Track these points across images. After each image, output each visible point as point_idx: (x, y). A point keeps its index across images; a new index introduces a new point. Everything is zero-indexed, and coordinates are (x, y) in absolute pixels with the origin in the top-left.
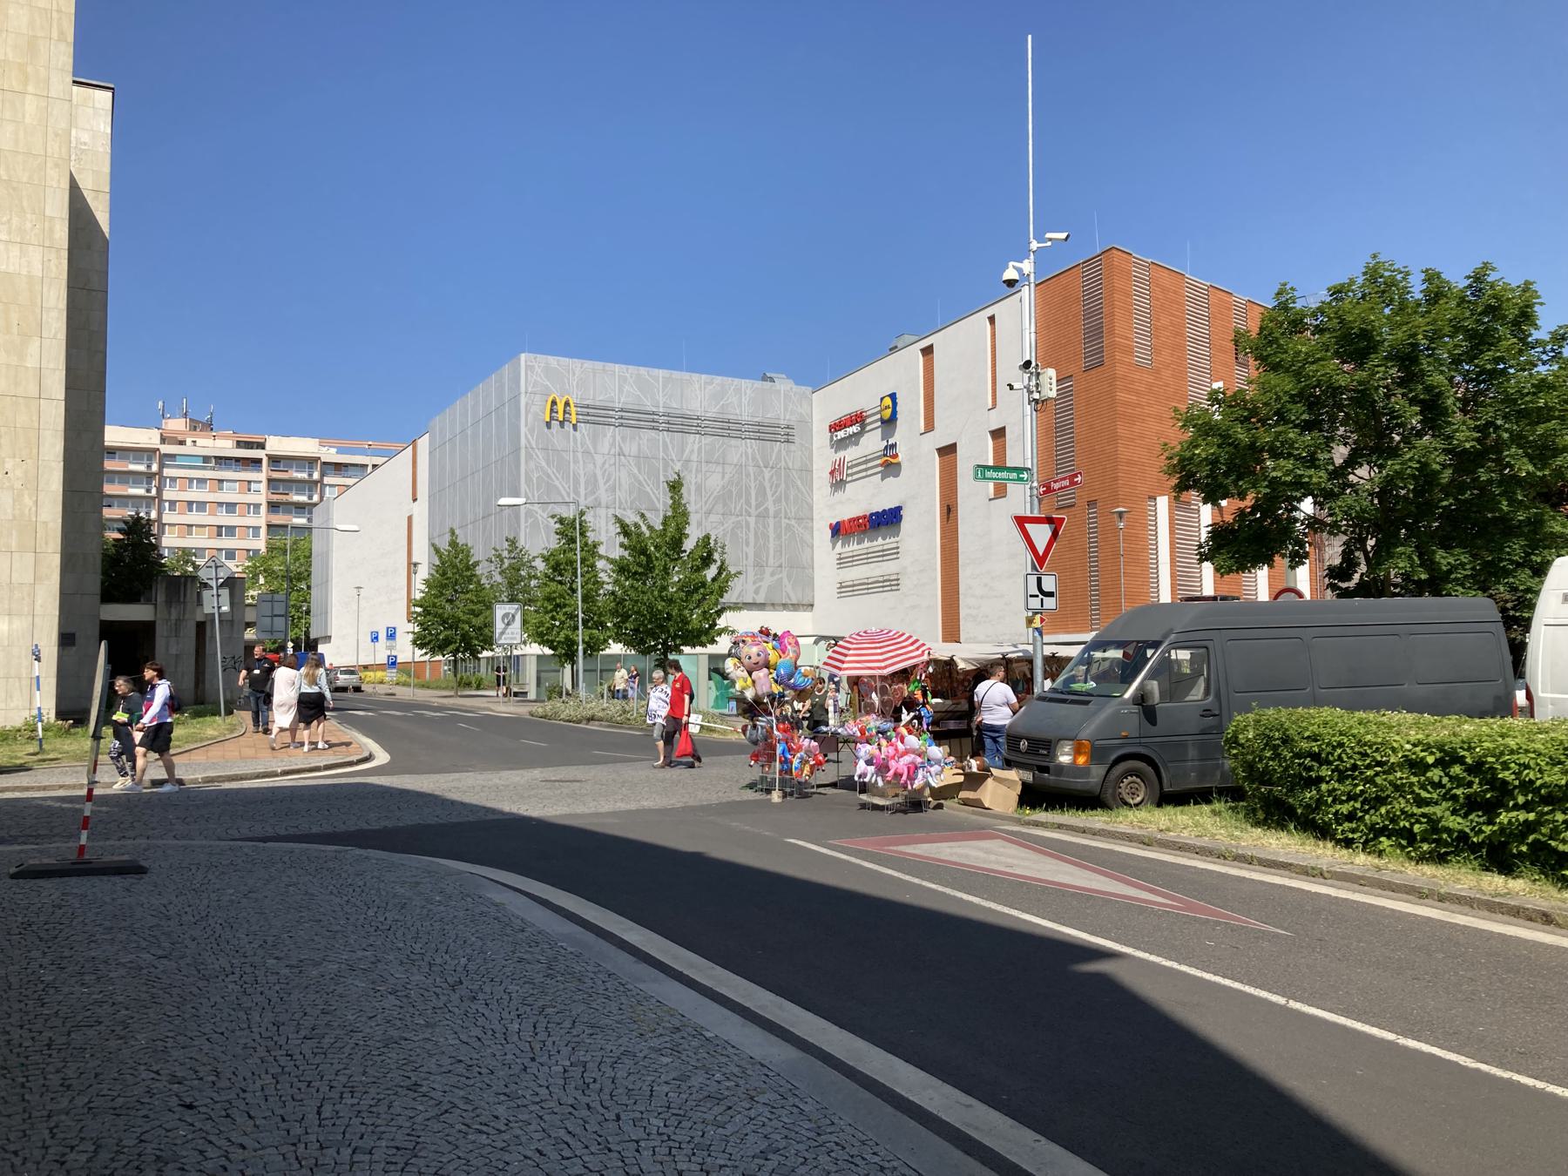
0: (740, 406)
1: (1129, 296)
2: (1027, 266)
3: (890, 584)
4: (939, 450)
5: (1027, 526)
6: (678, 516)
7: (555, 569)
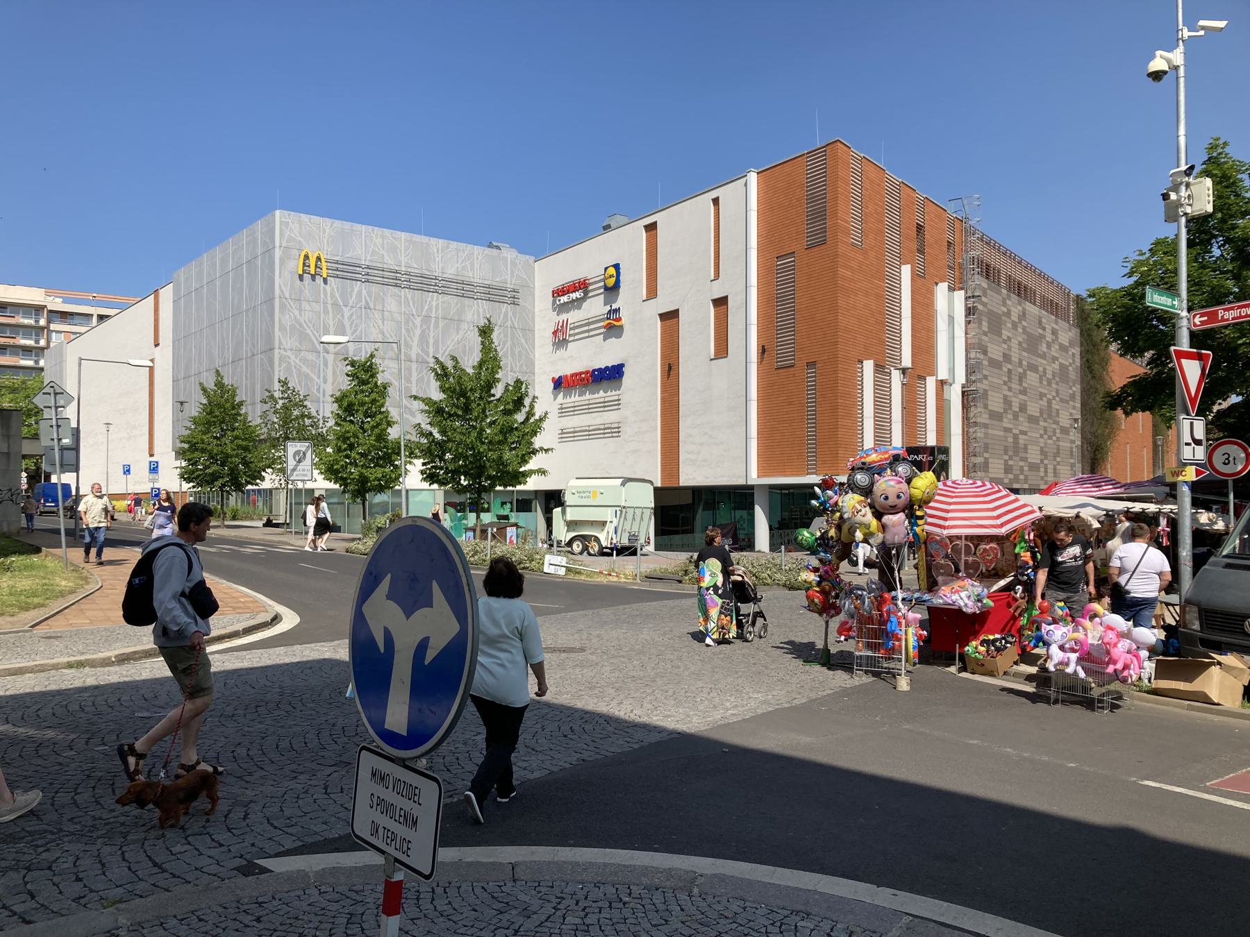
0: (472, 269)
1: (848, 185)
2: (1178, 56)
3: (613, 431)
4: (661, 316)
5: (1183, 361)
6: (490, 361)
7: (346, 410)
